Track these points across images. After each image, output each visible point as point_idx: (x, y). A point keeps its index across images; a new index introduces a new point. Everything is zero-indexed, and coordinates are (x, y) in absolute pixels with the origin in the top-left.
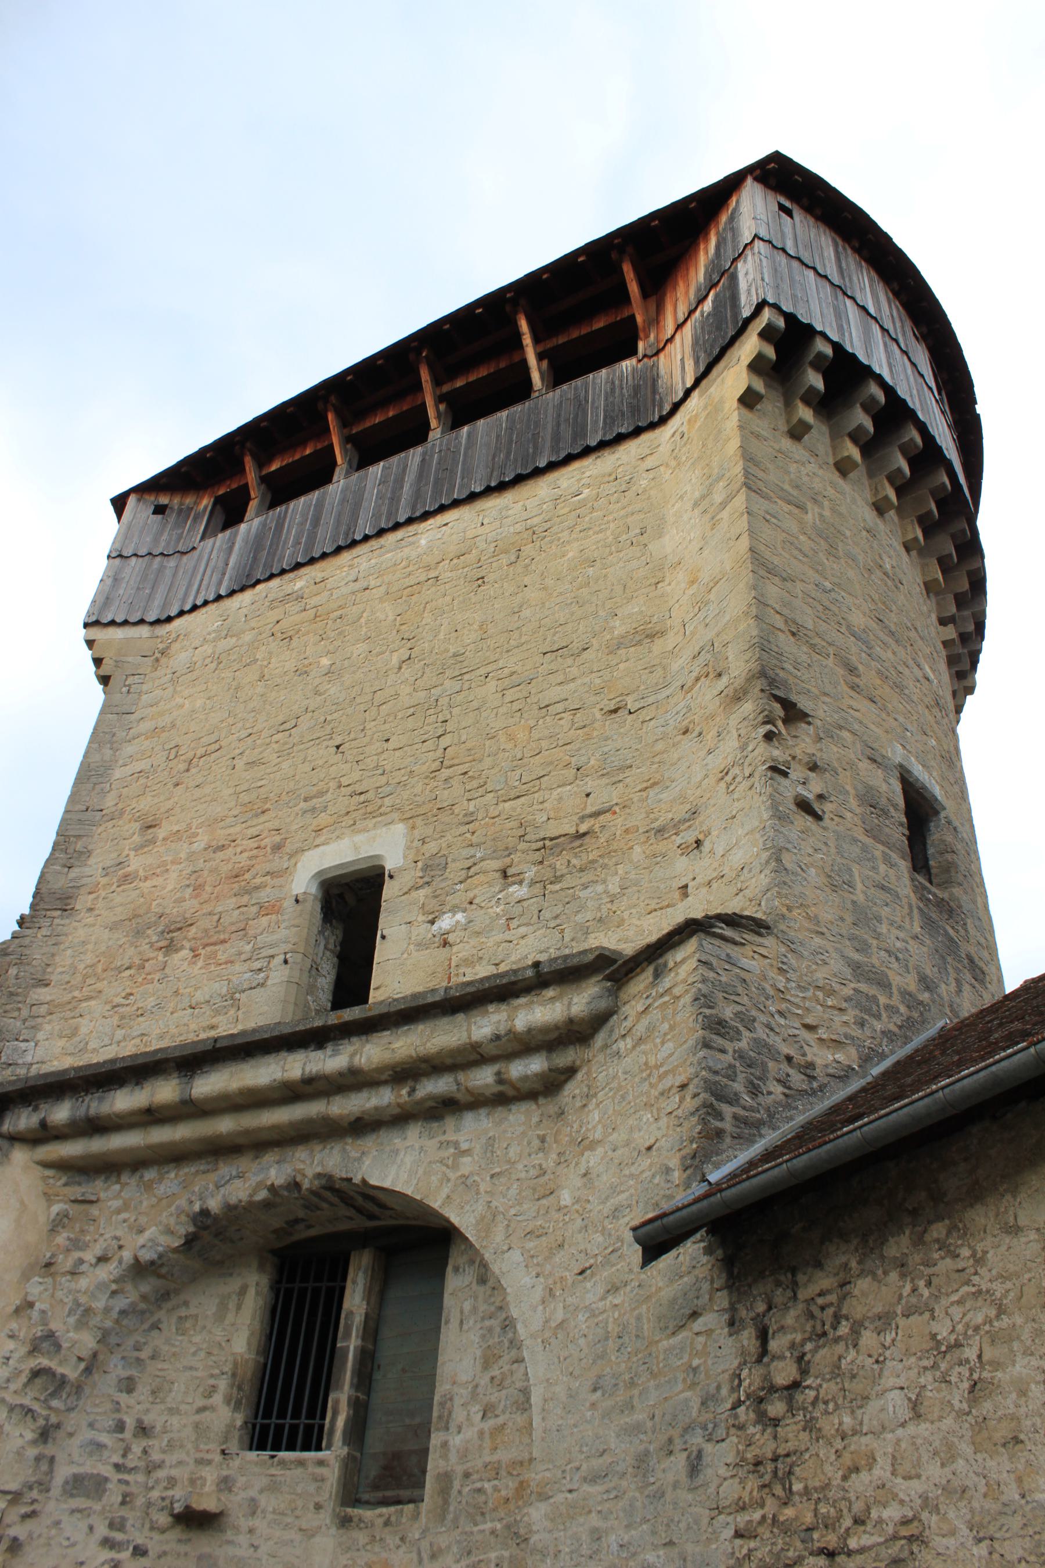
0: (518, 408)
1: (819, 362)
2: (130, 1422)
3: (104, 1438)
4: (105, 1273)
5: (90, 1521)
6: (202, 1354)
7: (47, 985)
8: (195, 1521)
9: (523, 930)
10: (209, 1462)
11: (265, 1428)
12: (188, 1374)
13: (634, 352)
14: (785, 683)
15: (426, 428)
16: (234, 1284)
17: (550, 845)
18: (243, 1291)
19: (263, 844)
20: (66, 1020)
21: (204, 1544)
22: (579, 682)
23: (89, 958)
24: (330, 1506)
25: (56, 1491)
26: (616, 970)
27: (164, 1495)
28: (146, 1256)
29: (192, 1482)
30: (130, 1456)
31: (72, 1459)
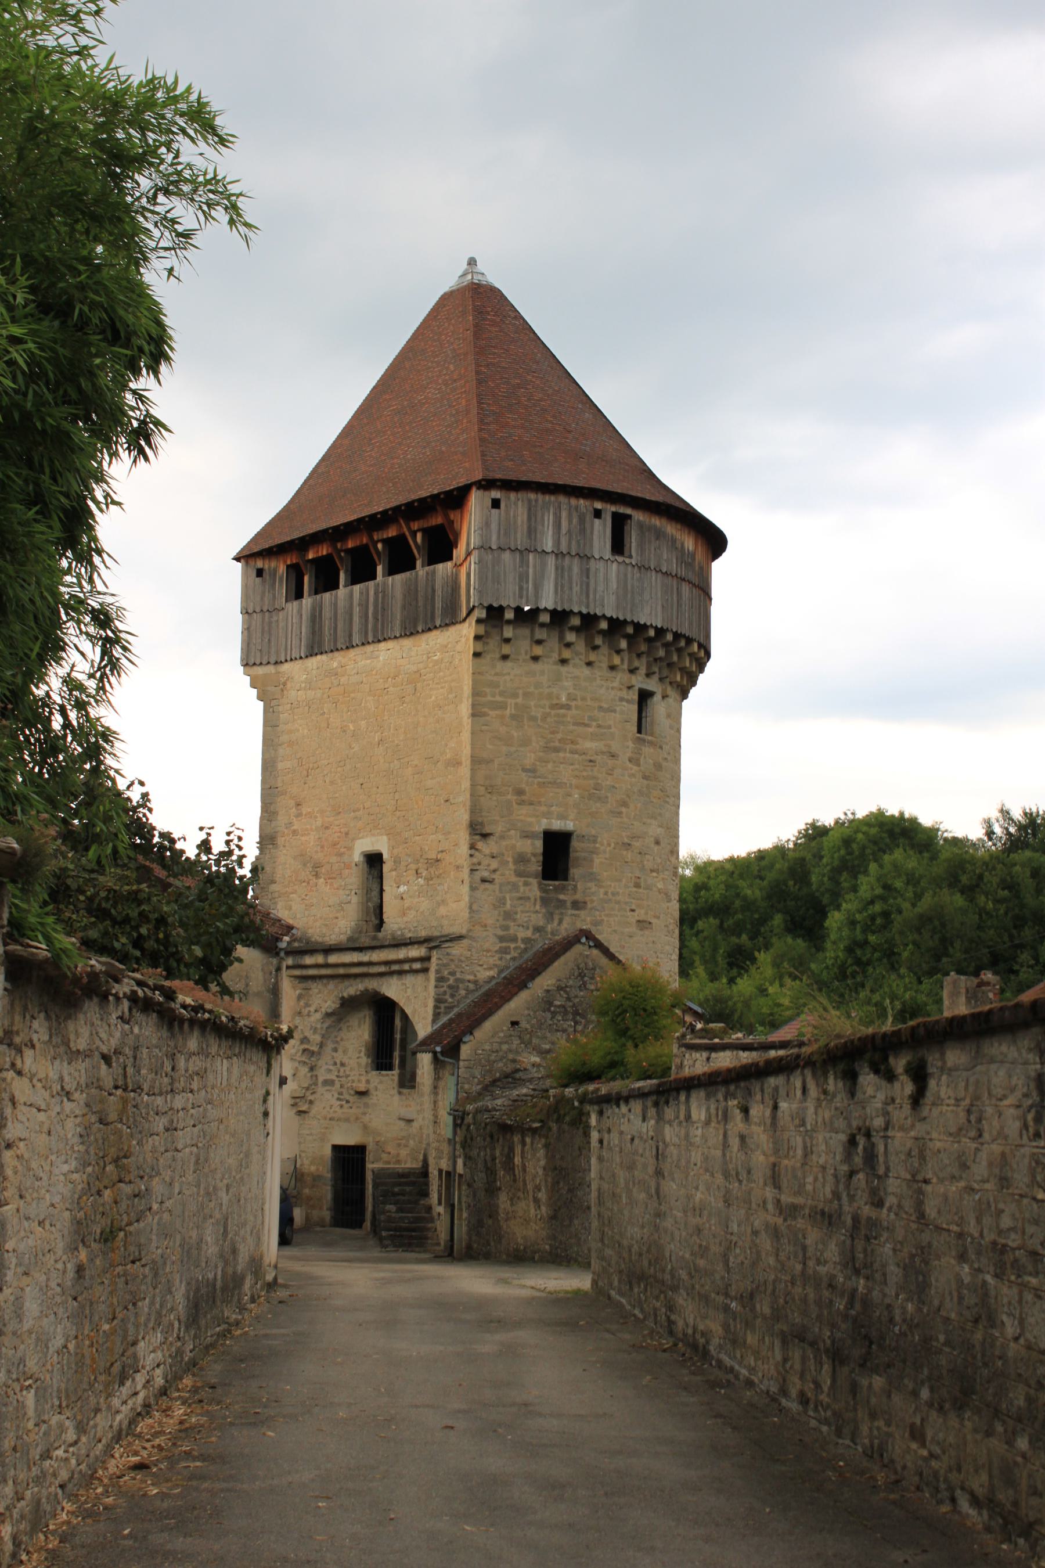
0: (408, 573)
3: (331, 1067)
4: (318, 1016)
14: (482, 824)
16: (362, 1015)
21: (365, 1099)
28: (329, 1011)
31: (322, 1075)
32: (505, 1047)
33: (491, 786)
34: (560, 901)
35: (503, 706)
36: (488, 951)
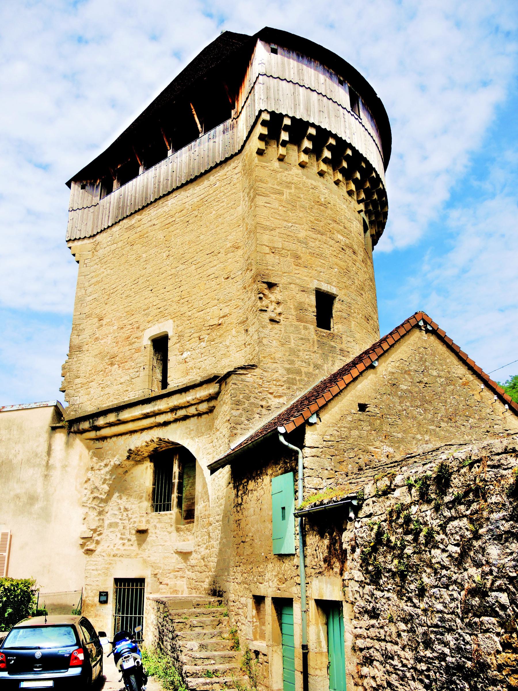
1: (287, 128)
2: (122, 507)
3: (116, 512)
8: (142, 532)
9: (205, 358)
11: (157, 506)
18: (147, 468)
19: (133, 327)
22: (217, 266)
23: (89, 368)
24: (174, 525)
25: (106, 527)
26: (221, 380)
29: (140, 522)
31: (108, 519)
32: (355, 433)
33: (274, 248)
34: (332, 347)
35: (281, 193)
36: (277, 380)
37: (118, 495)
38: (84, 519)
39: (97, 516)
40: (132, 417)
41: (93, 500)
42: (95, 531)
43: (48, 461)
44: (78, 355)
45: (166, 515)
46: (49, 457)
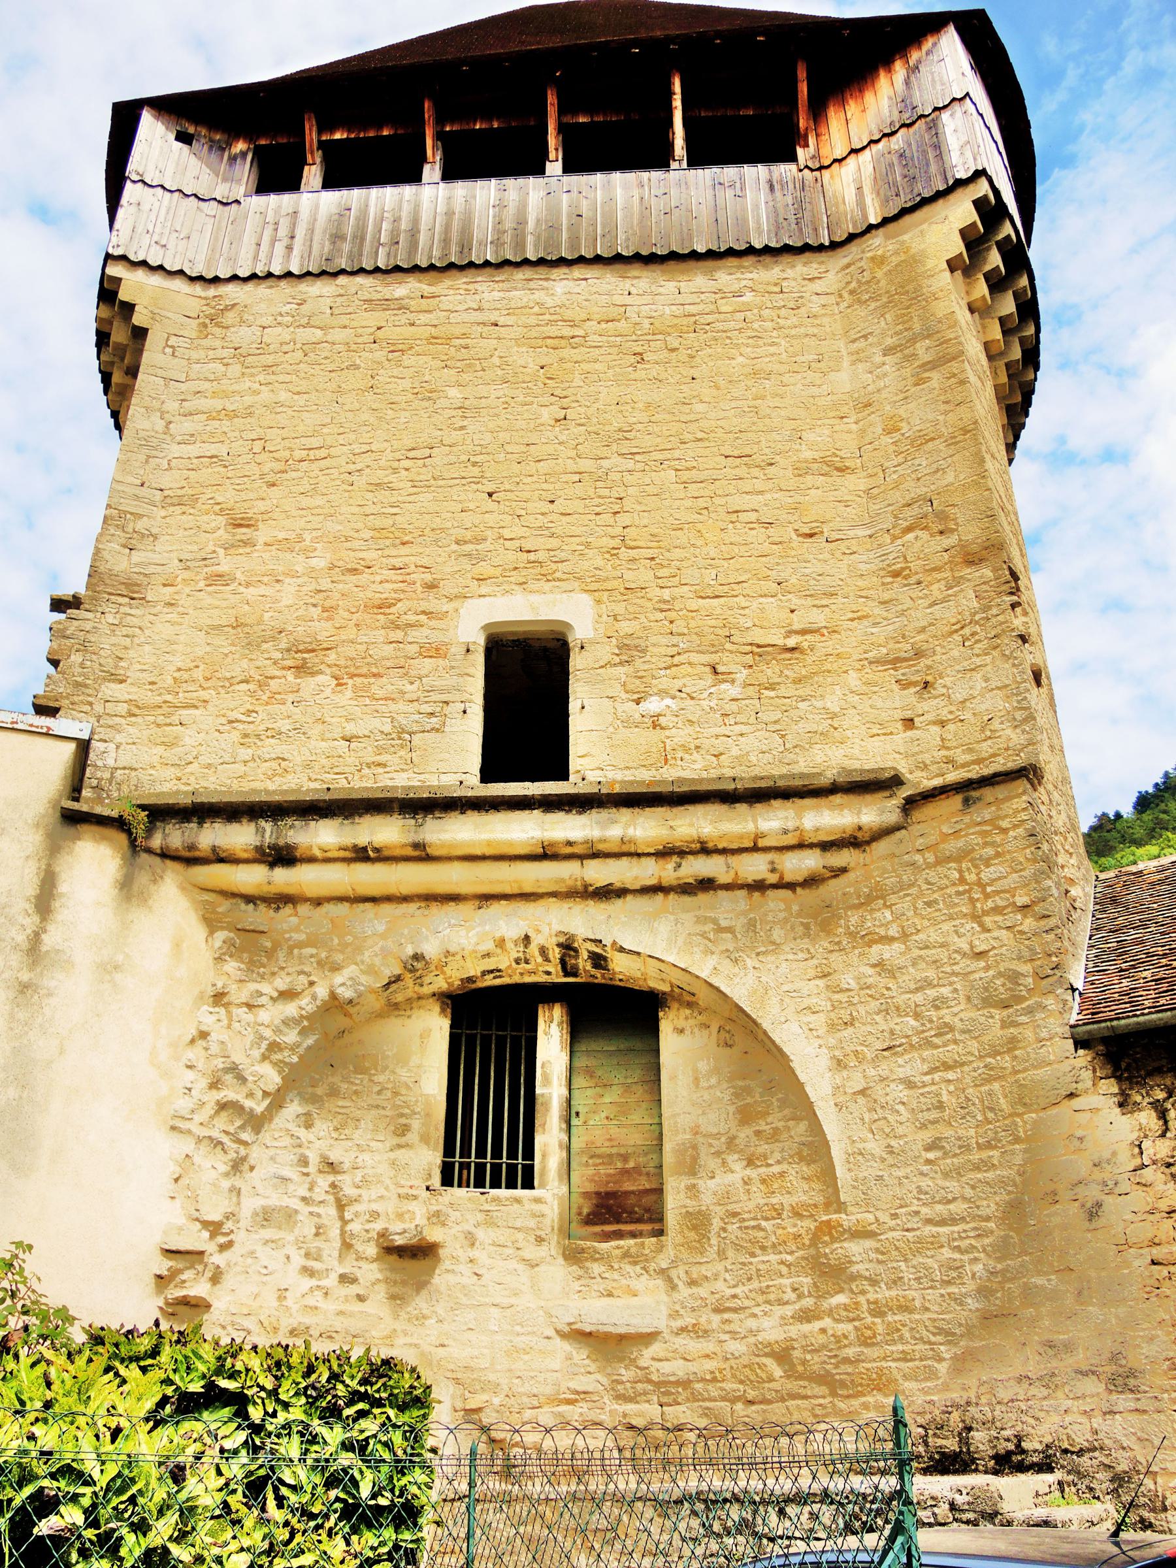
2: (314, 1158)
3: (287, 1172)
5: (285, 1251)
6: (389, 1094)
7: (121, 682)
10: (415, 1197)
12: (373, 1112)
13: (793, 158)
15: (543, 157)
17: (760, 651)
20: (159, 726)
27: (368, 1226)
30: (317, 1190)
31: (259, 1191)
37: (300, 1110)
38: (176, 1180)
39: (227, 1174)
40: (489, 843)
41: (217, 1112)
42: (214, 1228)
43: (37, 935)
44: (123, 609)
45: (518, 1201)
46: (44, 919)
